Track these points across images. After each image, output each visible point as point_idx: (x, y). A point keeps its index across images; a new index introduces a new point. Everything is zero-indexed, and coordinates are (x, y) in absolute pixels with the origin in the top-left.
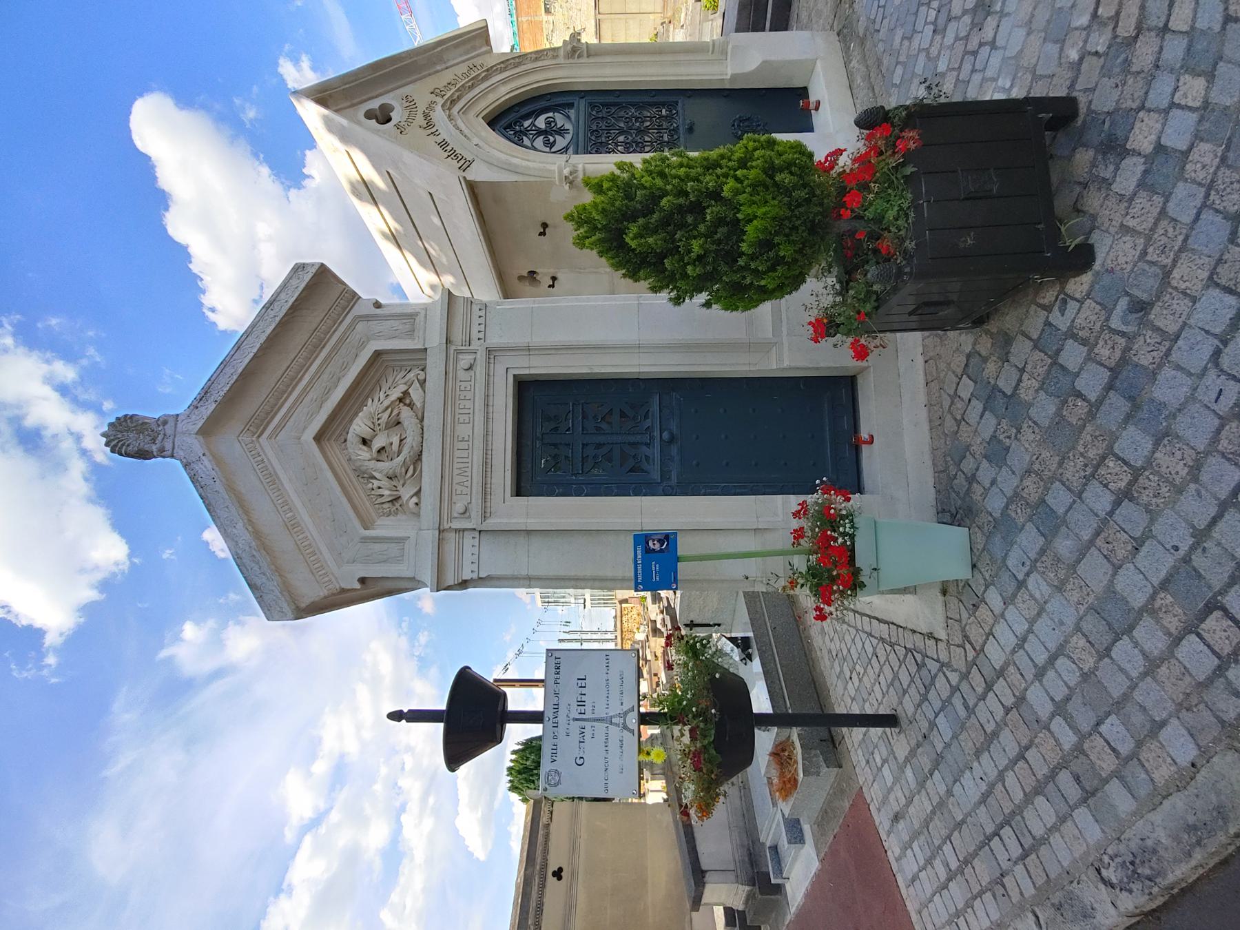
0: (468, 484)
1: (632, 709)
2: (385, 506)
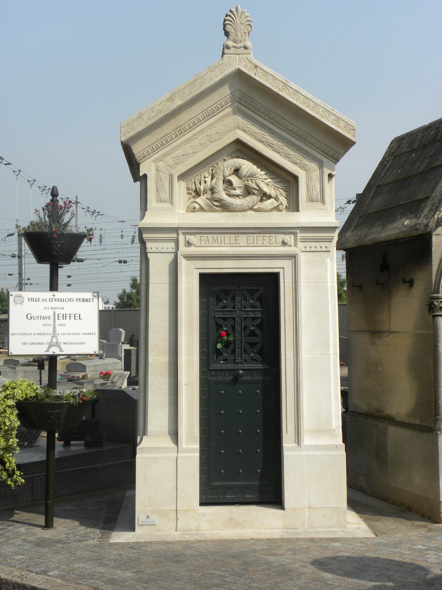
0: (208, 245)
1: (61, 351)
2: (194, 186)
